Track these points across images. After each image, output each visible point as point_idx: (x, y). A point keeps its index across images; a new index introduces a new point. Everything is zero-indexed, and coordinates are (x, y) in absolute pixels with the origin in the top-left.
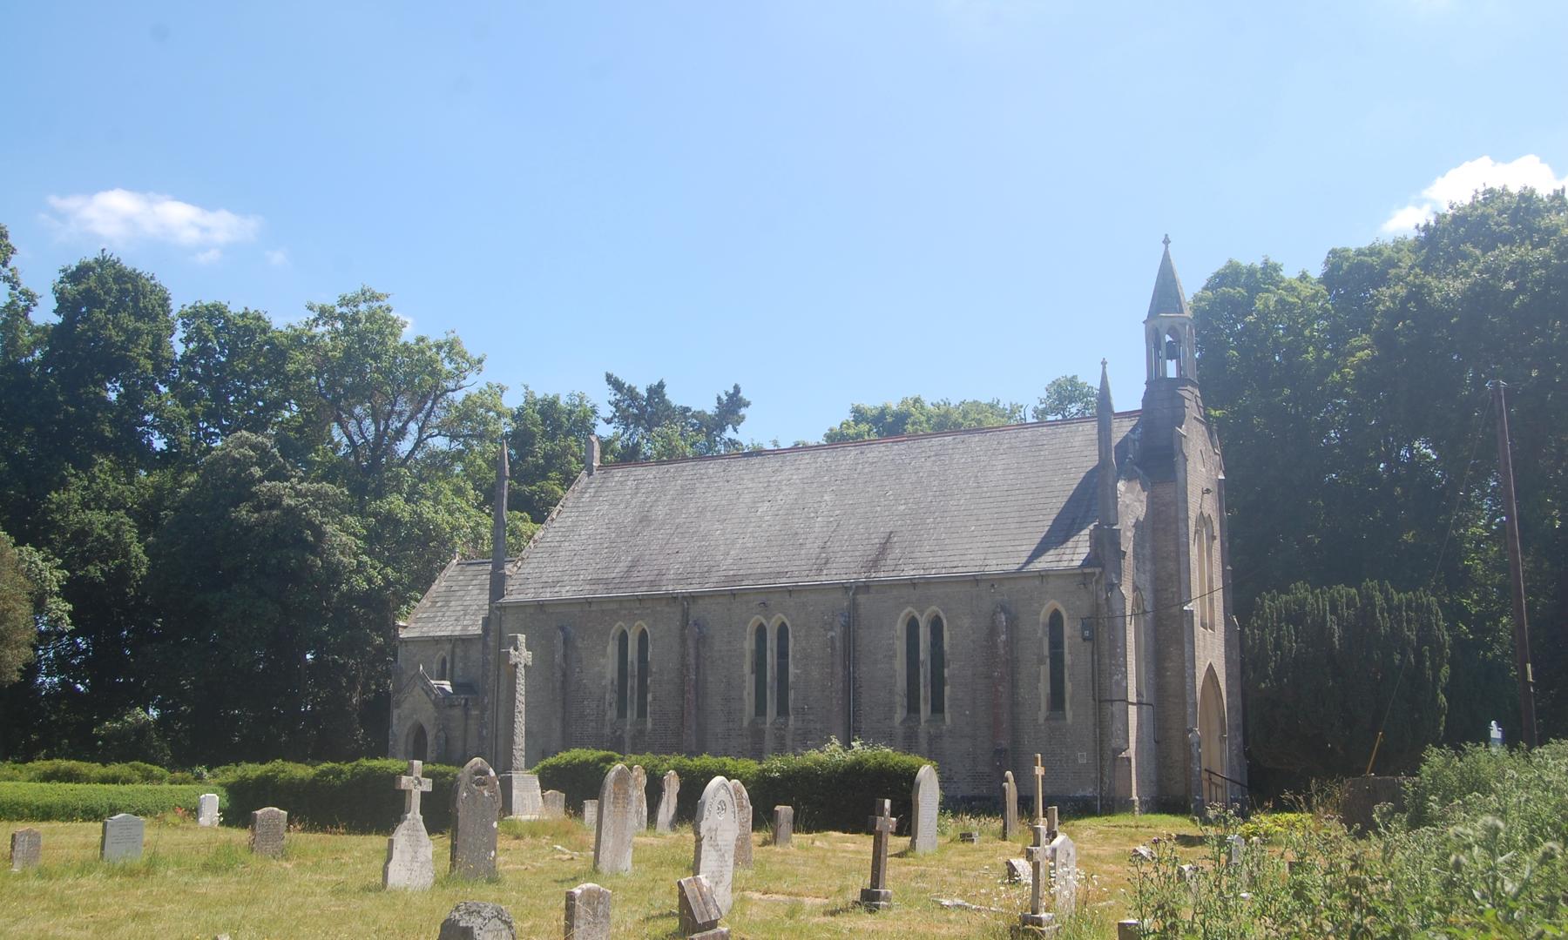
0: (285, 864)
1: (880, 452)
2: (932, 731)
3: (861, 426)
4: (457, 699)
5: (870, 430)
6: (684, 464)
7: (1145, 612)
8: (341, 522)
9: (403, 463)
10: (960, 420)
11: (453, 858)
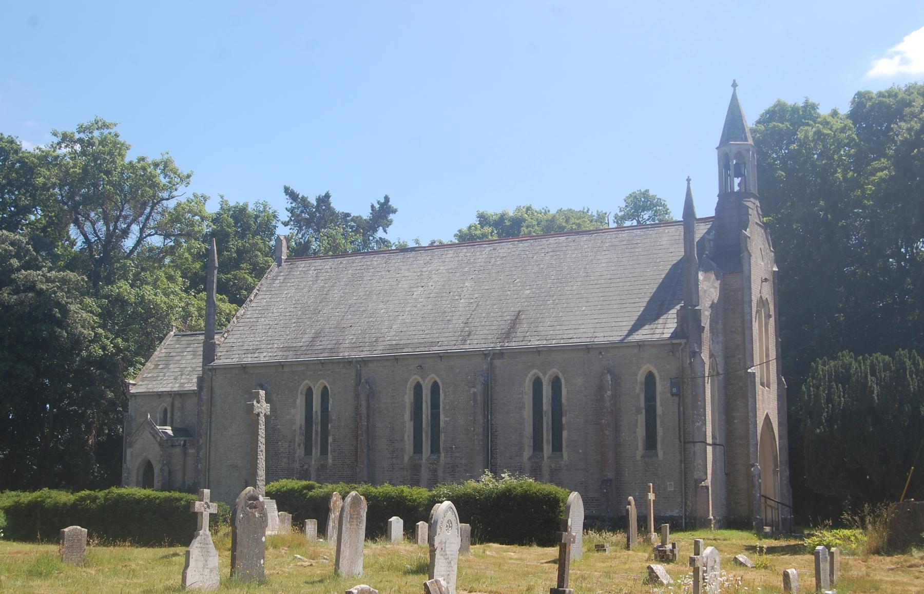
0: (89, 570)
1: (508, 248)
4: (177, 440)
5: (493, 232)
6: (354, 258)
7: (718, 374)
8: (81, 302)
9: (128, 256)
10: (564, 224)
11: (233, 565)
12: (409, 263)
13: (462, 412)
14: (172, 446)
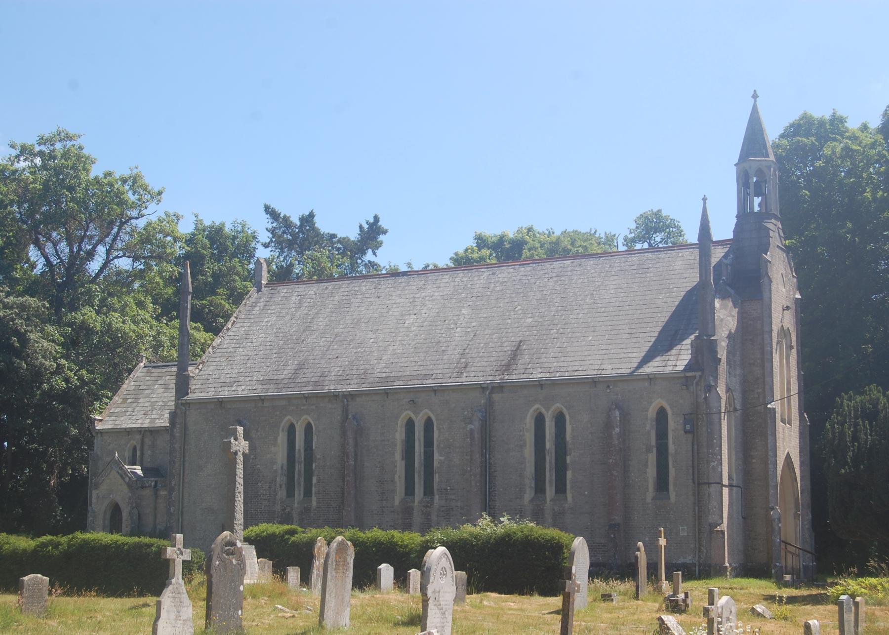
1: (509, 273)
2: (556, 508)
3: (483, 251)
4: (147, 481)
5: (491, 255)
6: (341, 283)
7: (735, 410)
9: (94, 281)
10: (569, 247)
11: (208, 616)
12: (400, 289)
13: (457, 450)
14: (142, 487)
